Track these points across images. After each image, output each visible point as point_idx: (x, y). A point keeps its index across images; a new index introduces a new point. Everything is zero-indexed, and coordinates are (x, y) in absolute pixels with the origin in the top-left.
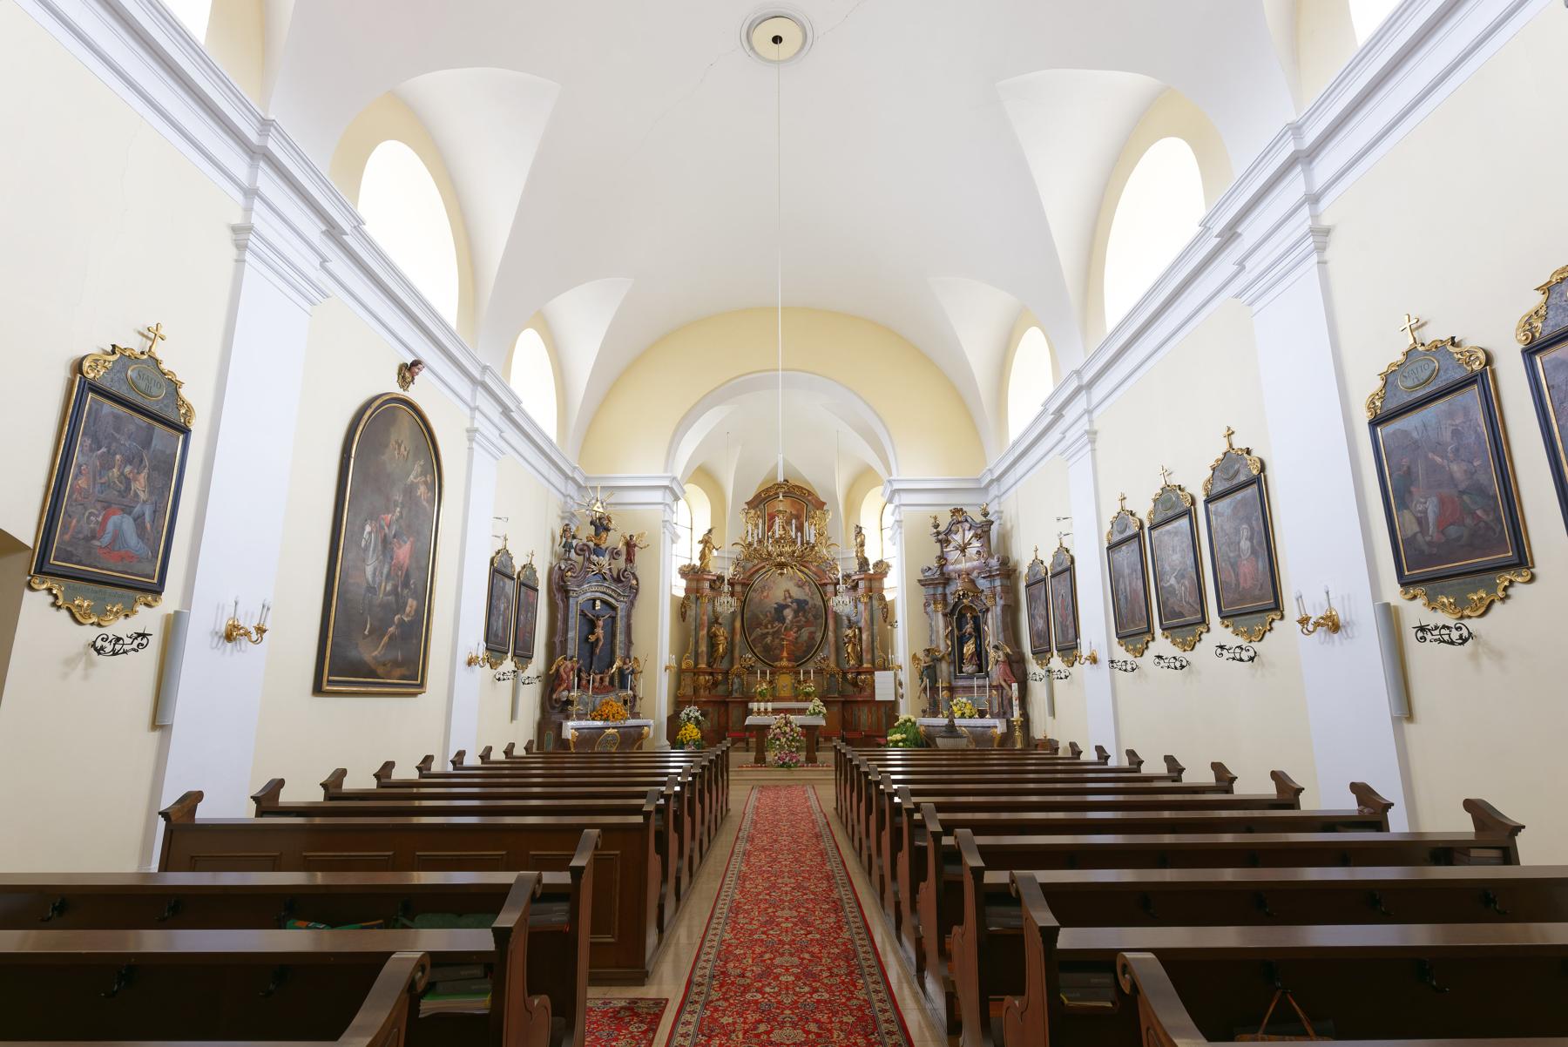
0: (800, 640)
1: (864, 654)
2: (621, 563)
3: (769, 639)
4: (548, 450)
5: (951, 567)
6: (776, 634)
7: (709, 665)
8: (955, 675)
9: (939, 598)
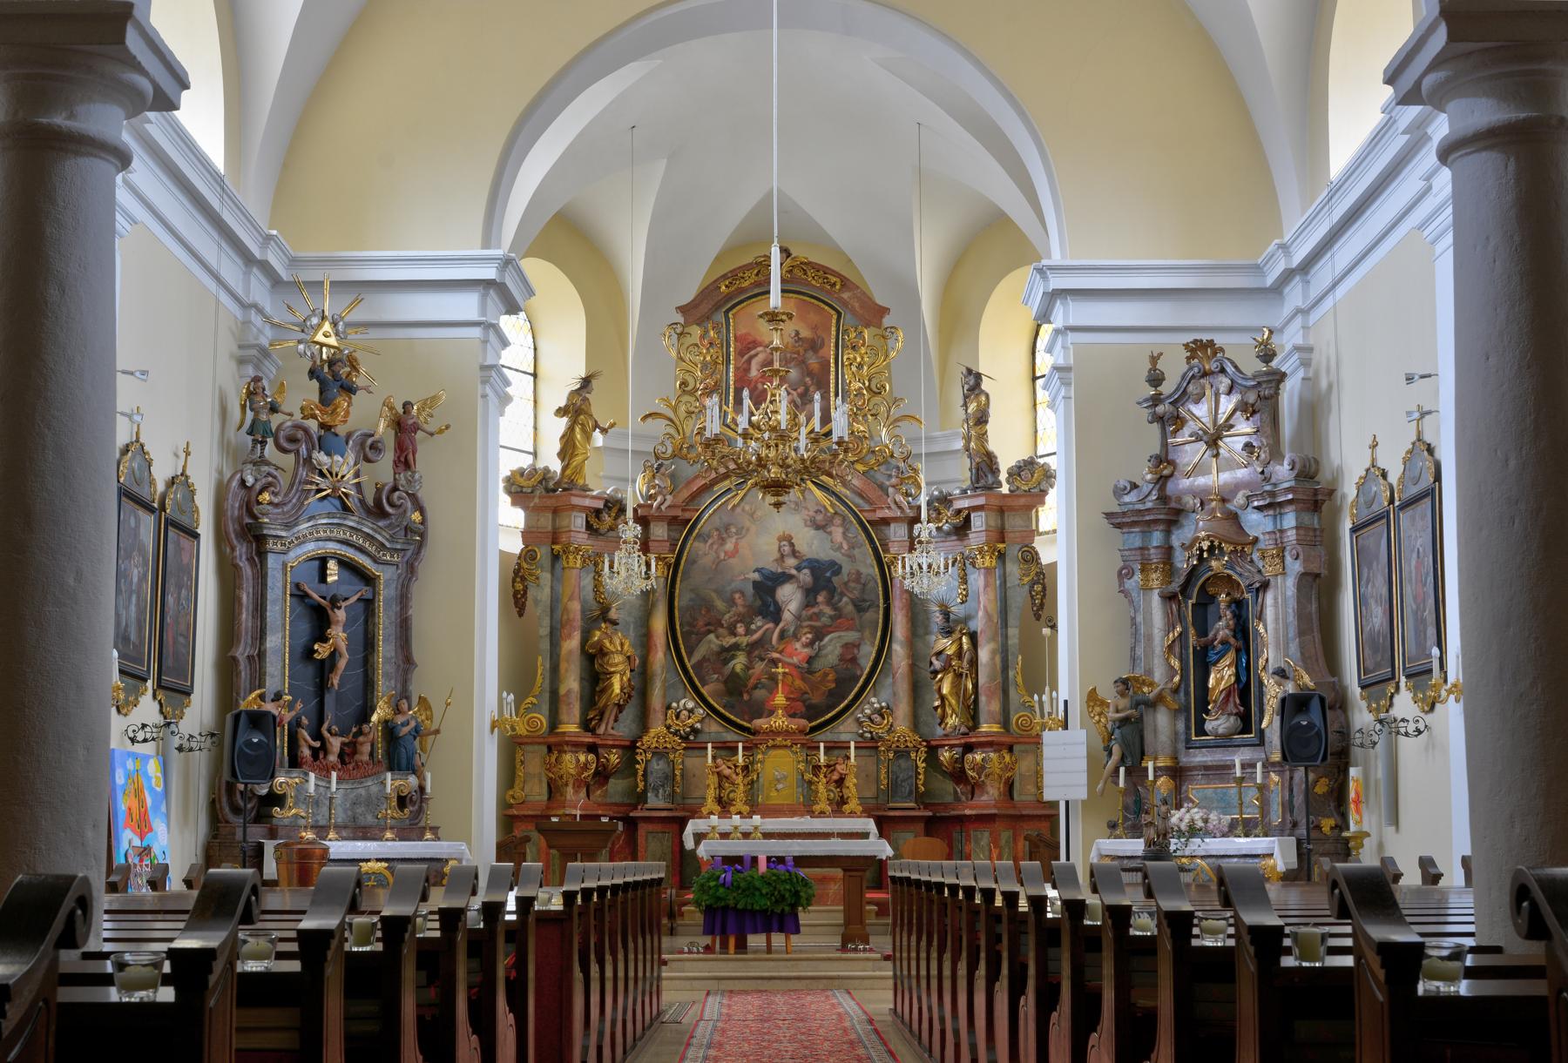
0: (819, 665)
1: (983, 699)
2: (384, 469)
3: (739, 663)
4: (215, 202)
5: (1185, 483)
6: (757, 648)
7: (586, 725)
8: (1188, 740)
9: (1155, 556)
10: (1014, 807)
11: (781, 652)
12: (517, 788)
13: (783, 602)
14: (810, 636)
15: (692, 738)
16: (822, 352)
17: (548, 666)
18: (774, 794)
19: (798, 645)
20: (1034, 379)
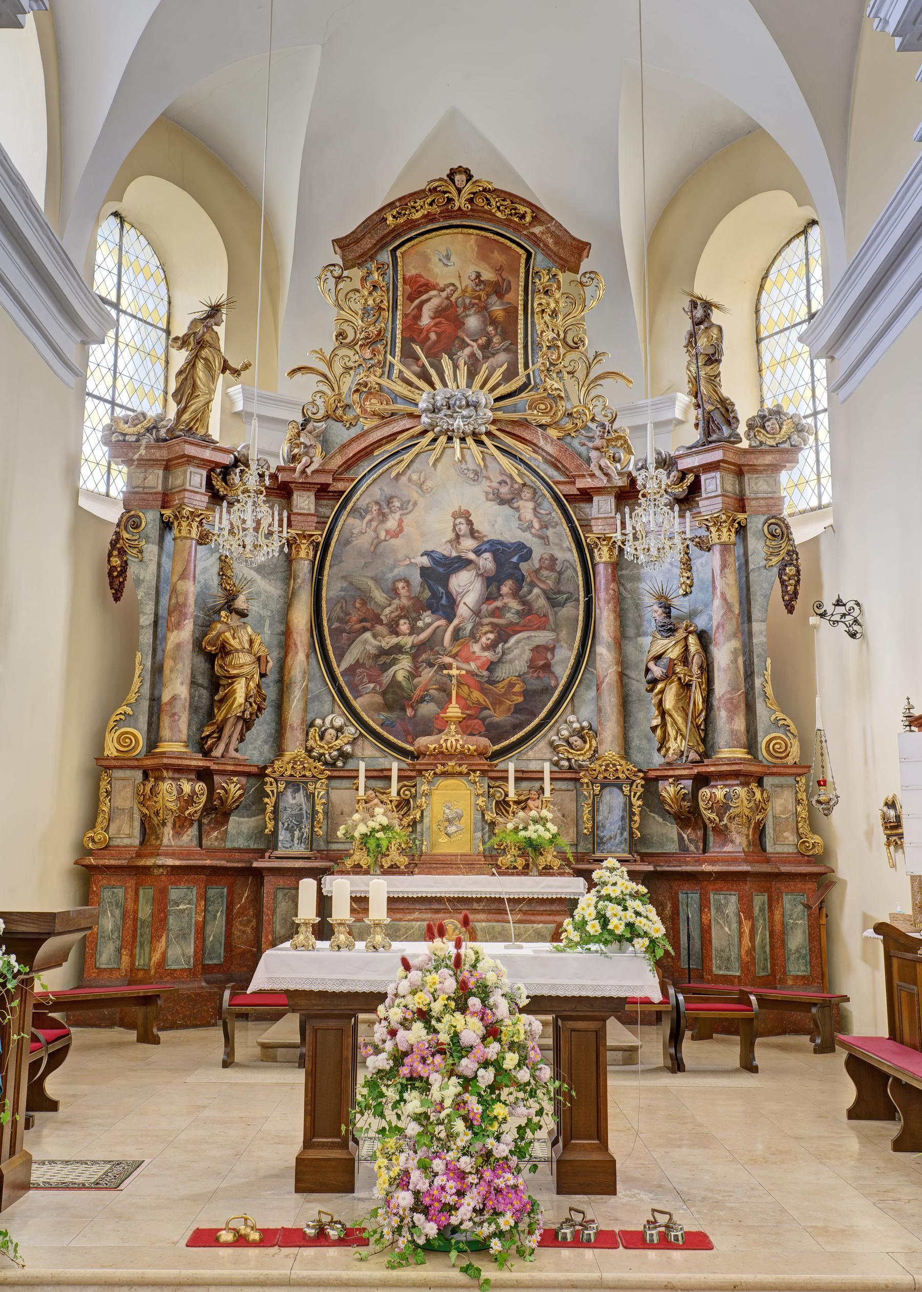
3: (401, 668)
10: (768, 861)
11: (454, 657)
12: (98, 829)
13: (458, 594)
14: (491, 636)
15: (340, 764)
16: (509, 297)
17: (149, 664)
18: (444, 839)
19: (476, 648)
20: (758, 341)
